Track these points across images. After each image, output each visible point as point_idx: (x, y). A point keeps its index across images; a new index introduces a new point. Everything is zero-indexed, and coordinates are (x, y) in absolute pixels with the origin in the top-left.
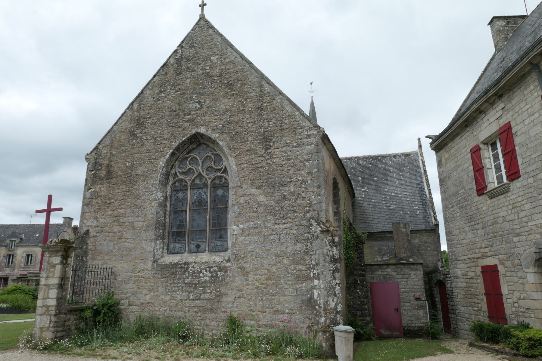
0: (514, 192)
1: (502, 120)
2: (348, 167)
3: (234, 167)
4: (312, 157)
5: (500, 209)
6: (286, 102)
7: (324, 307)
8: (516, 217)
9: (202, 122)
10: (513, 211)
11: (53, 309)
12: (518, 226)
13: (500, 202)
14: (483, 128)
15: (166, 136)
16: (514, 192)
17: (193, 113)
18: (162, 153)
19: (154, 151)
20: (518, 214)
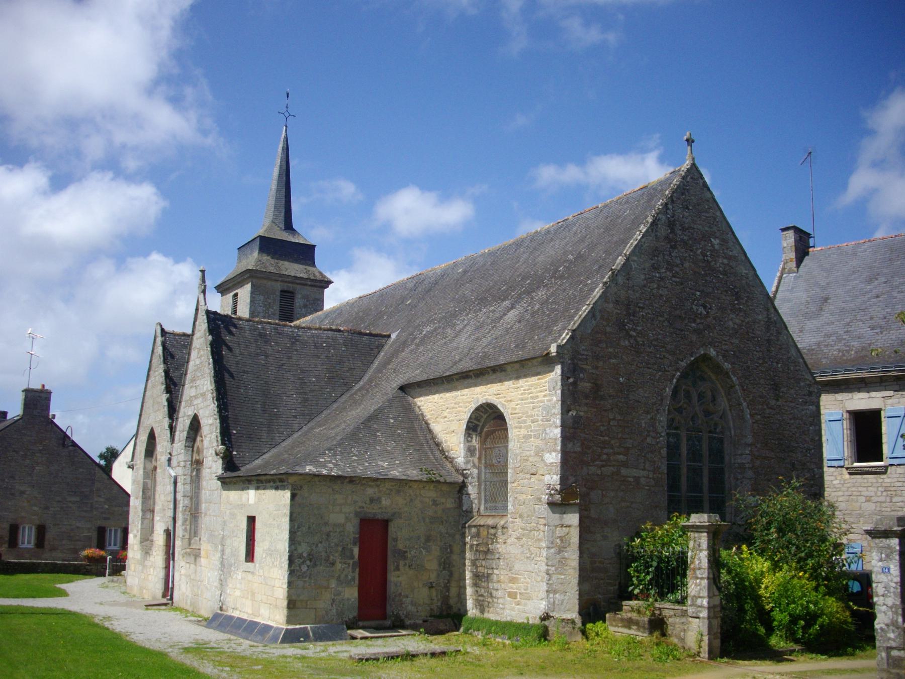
0: (890, 476)
1: (890, 400)
2: (321, 289)
3: (749, 416)
4: (814, 420)
5: (865, 488)
6: (790, 340)
7: (657, 568)
8: (888, 500)
9: (710, 340)
10: (885, 494)
11: (860, 568)
12: (889, 509)
13: (866, 481)
14: (857, 398)
15: (669, 347)
16: (890, 476)
17: (698, 321)
18: (666, 373)
19: (656, 367)
20: (891, 497)
